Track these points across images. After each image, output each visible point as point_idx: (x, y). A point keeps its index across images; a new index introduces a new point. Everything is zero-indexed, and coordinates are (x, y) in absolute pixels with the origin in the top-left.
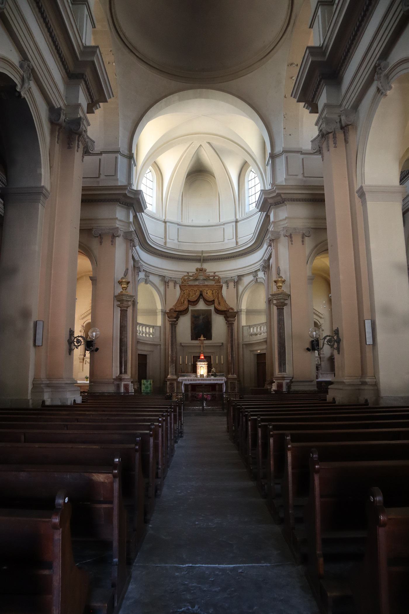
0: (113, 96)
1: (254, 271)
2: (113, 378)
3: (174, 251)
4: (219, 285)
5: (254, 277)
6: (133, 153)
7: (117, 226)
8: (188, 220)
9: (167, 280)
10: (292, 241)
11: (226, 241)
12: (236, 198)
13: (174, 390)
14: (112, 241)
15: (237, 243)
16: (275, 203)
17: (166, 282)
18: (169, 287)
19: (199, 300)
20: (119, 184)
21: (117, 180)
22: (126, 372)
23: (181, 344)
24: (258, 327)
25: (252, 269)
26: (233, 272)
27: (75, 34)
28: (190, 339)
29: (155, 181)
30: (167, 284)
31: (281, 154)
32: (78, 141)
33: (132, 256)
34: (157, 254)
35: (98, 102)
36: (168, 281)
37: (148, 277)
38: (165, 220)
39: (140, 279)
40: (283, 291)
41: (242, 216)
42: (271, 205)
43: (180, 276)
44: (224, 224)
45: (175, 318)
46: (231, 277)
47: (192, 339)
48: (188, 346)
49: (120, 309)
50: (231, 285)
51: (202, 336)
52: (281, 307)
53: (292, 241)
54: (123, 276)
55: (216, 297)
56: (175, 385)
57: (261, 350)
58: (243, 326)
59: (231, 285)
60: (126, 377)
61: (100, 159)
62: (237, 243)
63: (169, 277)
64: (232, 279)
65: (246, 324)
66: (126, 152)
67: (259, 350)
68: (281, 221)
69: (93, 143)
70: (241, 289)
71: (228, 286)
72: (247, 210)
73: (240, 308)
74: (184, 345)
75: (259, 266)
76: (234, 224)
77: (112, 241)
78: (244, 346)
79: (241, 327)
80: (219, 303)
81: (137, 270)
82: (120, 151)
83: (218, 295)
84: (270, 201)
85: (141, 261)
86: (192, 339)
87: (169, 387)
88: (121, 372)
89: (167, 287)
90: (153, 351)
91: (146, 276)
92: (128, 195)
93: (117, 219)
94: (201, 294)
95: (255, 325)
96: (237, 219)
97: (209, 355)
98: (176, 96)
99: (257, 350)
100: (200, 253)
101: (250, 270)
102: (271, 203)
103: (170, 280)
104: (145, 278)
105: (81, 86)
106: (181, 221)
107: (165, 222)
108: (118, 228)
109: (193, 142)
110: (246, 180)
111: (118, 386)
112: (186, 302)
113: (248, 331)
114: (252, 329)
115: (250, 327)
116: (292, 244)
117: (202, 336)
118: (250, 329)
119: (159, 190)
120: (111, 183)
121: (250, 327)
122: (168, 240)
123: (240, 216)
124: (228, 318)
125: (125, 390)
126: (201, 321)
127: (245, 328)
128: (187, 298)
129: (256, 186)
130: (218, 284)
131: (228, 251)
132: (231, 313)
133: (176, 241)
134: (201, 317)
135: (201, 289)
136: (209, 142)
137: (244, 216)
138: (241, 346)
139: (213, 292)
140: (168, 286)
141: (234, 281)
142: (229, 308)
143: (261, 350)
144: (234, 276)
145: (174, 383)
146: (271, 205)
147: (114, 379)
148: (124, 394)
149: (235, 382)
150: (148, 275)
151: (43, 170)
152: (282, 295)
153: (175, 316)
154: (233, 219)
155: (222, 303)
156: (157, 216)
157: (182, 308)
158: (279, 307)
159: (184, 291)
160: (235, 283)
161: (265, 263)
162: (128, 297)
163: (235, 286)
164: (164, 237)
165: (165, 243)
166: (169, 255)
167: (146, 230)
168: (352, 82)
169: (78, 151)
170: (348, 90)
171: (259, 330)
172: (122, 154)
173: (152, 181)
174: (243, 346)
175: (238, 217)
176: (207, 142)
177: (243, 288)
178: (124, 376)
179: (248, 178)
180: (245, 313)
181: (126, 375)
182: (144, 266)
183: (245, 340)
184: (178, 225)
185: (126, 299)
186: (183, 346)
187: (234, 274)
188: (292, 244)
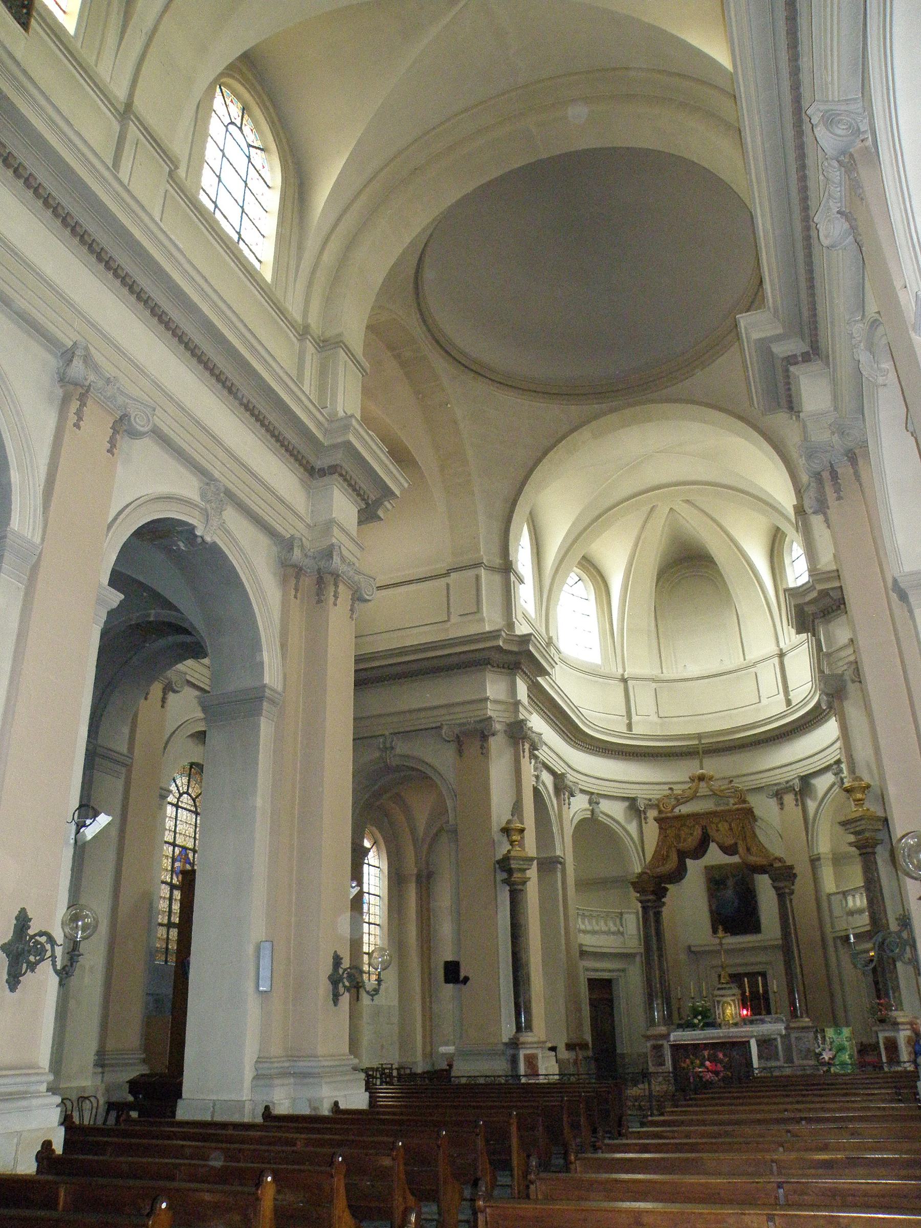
2: (504, 1041)
3: (652, 740)
5: (835, 774)
7: (490, 713)
8: (676, 668)
11: (764, 701)
12: (771, 603)
15: (789, 702)
16: (821, 611)
20: (487, 629)
21: (482, 620)
22: (529, 1027)
25: (829, 758)
26: (789, 768)
30: (643, 816)
32: (336, 585)
35: (378, 503)
37: (598, 803)
38: (623, 675)
39: (574, 816)
40: (868, 810)
41: (745, 660)
43: (656, 794)
44: (754, 665)
46: (787, 782)
50: (789, 799)
52: (869, 850)
58: (829, 895)
59: (789, 799)
60: (530, 1039)
61: (448, 585)
62: (789, 702)
64: (788, 788)
65: (837, 886)
66: (497, 561)
68: (841, 649)
69: (372, 580)
70: (812, 805)
71: (782, 804)
73: (816, 853)
74: (698, 949)
75: (838, 751)
76: (776, 660)
79: (825, 898)
80: (748, 850)
82: (483, 563)
84: (809, 610)
88: (519, 1029)
89: (643, 821)
90: (623, 970)
91: (590, 802)
93: (487, 699)
98: (585, 433)
99: (867, 951)
100: (694, 738)
101: (824, 760)
107: (624, 681)
108: (490, 718)
110: (787, 561)
111: (514, 1061)
113: (842, 904)
114: (850, 899)
115: (845, 894)
120: (472, 629)
121: (845, 894)
123: (787, 641)
125: (528, 1068)
127: (833, 898)
128: (675, 846)
130: (740, 806)
131: (766, 724)
132: (779, 869)
133: (654, 718)
135: (704, 823)
138: (830, 943)
139: (730, 825)
141: (794, 790)
142: (772, 857)
144: (791, 778)
147: (506, 1044)
148: (506, 1081)
151: (265, 655)
152: (863, 822)
155: (754, 850)
156: (605, 670)
158: (864, 851)
160: (796, 795)
162: (521, 863)
163: (797, 800)
165: (630, 726)
169: (335, 605)
176: (683, 501)
177: (817, 803)
178: (527, 1037)
180: (830, 863)
181: (530, 1034)
182: (580, 782)
184: (654, 680)
185: (517, 866)
186: (693, 952)
187: (792, 775)
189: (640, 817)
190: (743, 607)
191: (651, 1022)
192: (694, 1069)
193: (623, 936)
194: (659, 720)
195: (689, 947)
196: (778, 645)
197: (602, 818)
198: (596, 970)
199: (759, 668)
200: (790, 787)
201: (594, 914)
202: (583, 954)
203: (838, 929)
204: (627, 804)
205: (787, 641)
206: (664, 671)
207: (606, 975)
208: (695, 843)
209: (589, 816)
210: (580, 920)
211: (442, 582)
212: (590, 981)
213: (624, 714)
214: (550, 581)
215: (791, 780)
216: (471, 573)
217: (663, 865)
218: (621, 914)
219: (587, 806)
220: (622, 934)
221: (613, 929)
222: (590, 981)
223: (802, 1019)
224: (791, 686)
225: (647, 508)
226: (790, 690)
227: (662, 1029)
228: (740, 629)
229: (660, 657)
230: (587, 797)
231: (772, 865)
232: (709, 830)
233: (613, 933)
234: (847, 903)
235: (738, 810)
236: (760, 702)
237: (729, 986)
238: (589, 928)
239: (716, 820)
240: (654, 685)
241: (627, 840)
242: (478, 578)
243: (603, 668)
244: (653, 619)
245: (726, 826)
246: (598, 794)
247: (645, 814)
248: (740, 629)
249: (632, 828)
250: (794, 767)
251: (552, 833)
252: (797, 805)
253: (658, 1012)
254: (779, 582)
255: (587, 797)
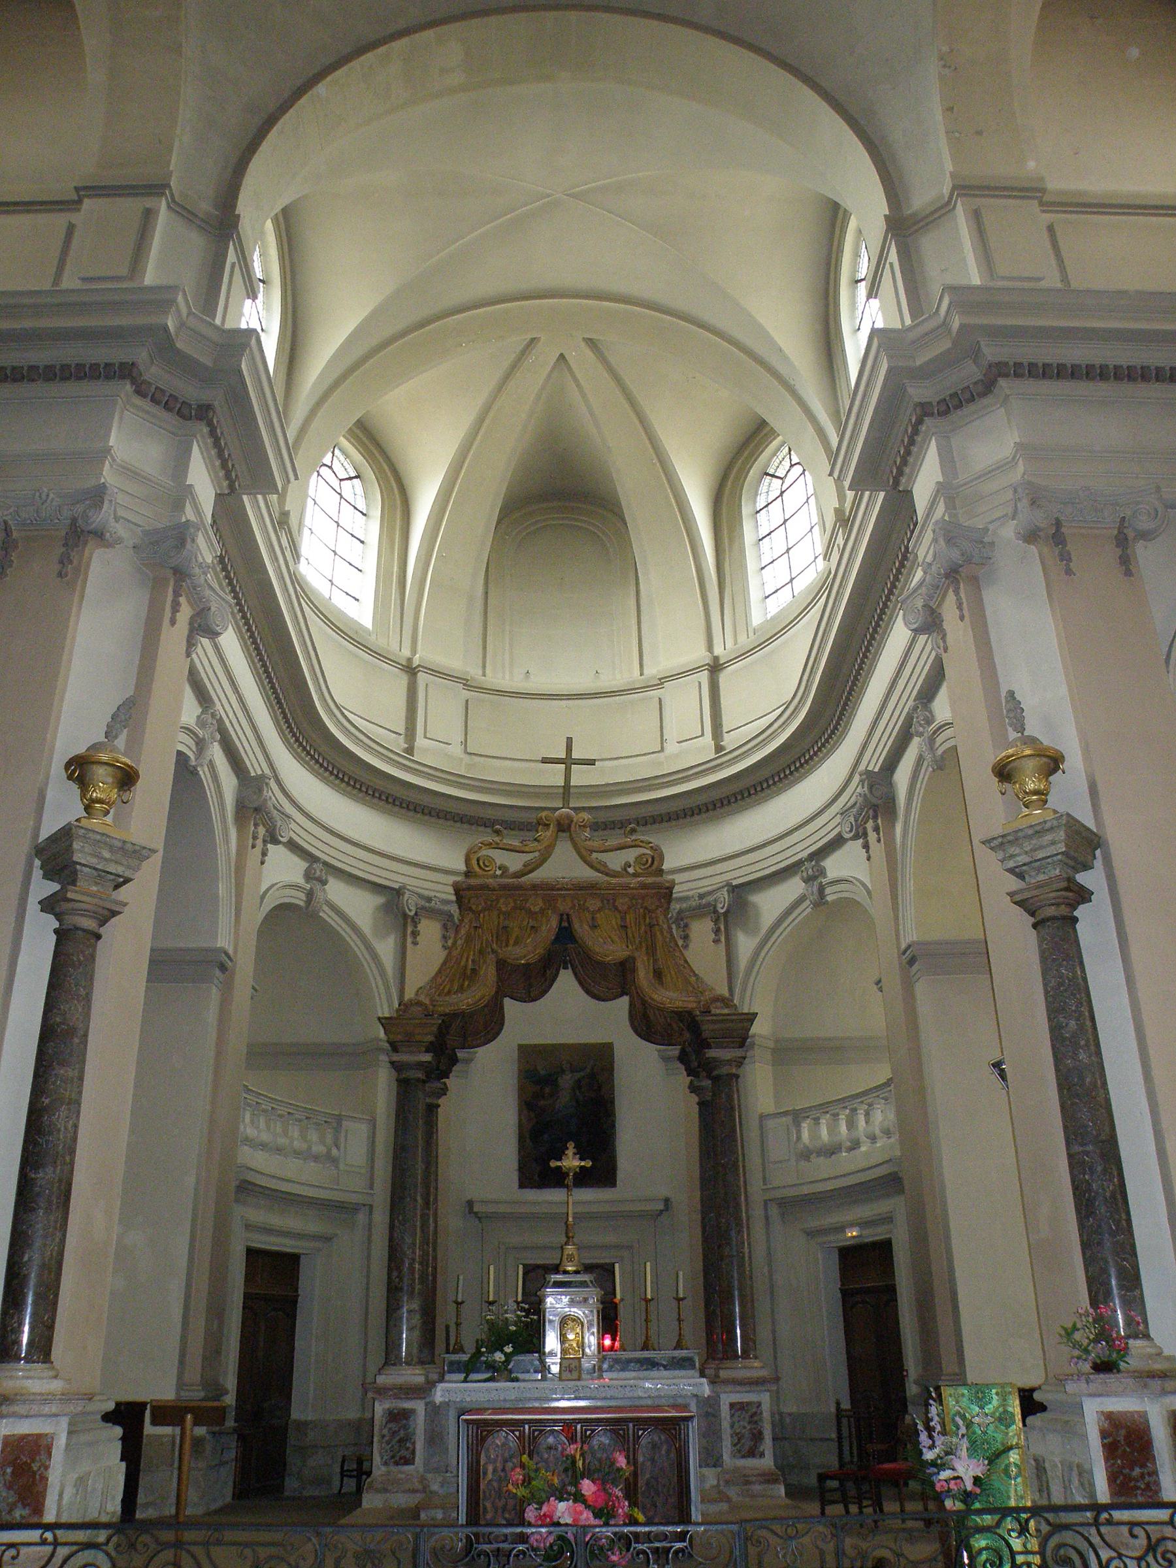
0: (297, 478)
1: (805, 854)
4: (658, 886)
5: (808, 880)
6: (239, 216)
9: (414, 909)
10: (1065, 557)
11: (671, 748)
13: (413, 1452)
14: (64, 560)
15: (719, 748)
17: (405, 916)
18: (418, 938)
19: (556, 975)
23: (471, 1211)
24: (838, 1115)
27: (292, 603)
28: (516, 1185)
29: (376, 513)
31: (943, 211)
33: (190, 672)
34: (364, 789)
36: (416, 914)
38: (410, 660)
42: (925, 411)
45: (427, 1051)
46: (701, 896)
47: (522, 1185)
48: (504, 1217)
49: (56, 925)
51: (570, 1151)
53: (1065, 557)
54: (102, 739)
55: (640, 943)
56: (419, 1424)
57: (863, 1224)
58: (762, 1117)
63: (421, 896)
67: (852, 1225)
70: (745, 944)
72: (757, 619)
76: (704, 677)
77: (64, 560)
78: (774, 1211)
81: (256, 825)
83: (653, 936)
84: (919, 392)
85: (272, 783)
86: (522, 1185)
87: (383, 1436)
89: (409, 940)
90: (328, 1239)
91: (308, 876)
92: (179, 345)
94: (565, 934)
95: (824, 1107)
96: (716, 659)
97: (602, 1258)
99: (841, 1229)
102: (922, 405)
103: (423, 908)
104: (308, 886)
105: (198, 442)
106: (480, 672)
107: (411, 670)
109: (533, 340)
112: (489, 973)
114: (805, 1126)
115: (797, 1116)
116: (1069, 572)
117: (570, 1151)
118: (798, 1126)
119: (392, 548)
121: (797, 1116)
122: (420, 742)
123: (729, 644)
124: (709, 1046)
126: (564, 1099)
127: (770, 1124)
129: (787, 523)
130: (650, 880)
133: (456, 750)
134: (566, 1081)
136: (590, 339)
137: (745, 641)
139: (623, 919)
140: (415, 934)
141: (715, 911)
143: (863, 1224)
145: (413, 1411)
146: (925, 411)
149: (759, 1404)
150: (318, 873)
153: (430, 1038)
154: (698, 654)
156: (379, 643)
157: (467, 1000)
159: (477, 914)
160: (716, 921)
161: (871, 788)
163: (717, 931)
164: (407, 728)
166: (426, 800)
167: (310, 648)
168: (880, 712)
170: (900, 669)
171: (843, 1128)
172: (178, 205)
173: (364, 515)
174: (766, 1210)
175: (718, 650)
179: (755, 502)
183: (777, 1183)
185: (93, 861)
188: (1069, 572)
189: (405, 926)
190: (652, 580)
191: (390, 1357)
192: (951, 1396)
193: (337, 1167)
194: (463, 756)
195: (470, 1203)
196: (710, 648)
197: (327, 915)
198: (269, 1231)
199: (669, 692)
200: (708, 905)
201: (282, 1110)
202: (246, 1189)
203: (776, 1183)
204: (380, 900)
205: (729, 644)
206: (488, 671)
207: (286, 1245)
208: (532, 958)
209: (302, 903)
210: (248, 1116)
211: (60, 220)
212: (251, 1253)
213: (402, 730)
214: (308, 408)
215: (710, 893)
216: (132, 206)
217: (461, 989)
218: (339, 1119)
219: (300, 880)
220: (334, 1161)
221: (318, 1149)
222: (251, 1253)
223: (747, 1362)
224: (727, 724)
225: (516, 341)
226: (725, 730)
227: (414, 1376)
228: (639, 623)
229: (485, 648)
230: (305, 865)
231: (707, 1012)
232: (576, 926)
233: (316, 1158)
234: (799, 1132)
235: (644, 886)
236: (662, 750)
237: (579, 1278)
238: (265, 1137)
239: (593, 904)
240: (466, 694)
241: (370, 969)
242: (149, 215)
243: (373, 637)
244: (481, 581)
245: (615, 922)
246: (326, 864)
247: (415, 924)
248: (639, 623)
249: (386, 948)
250: (719, 868)
251: (216, 897)
252: (716, 941)
253: (410, 1330)
254: (726, 541)
255: (305, 865)
